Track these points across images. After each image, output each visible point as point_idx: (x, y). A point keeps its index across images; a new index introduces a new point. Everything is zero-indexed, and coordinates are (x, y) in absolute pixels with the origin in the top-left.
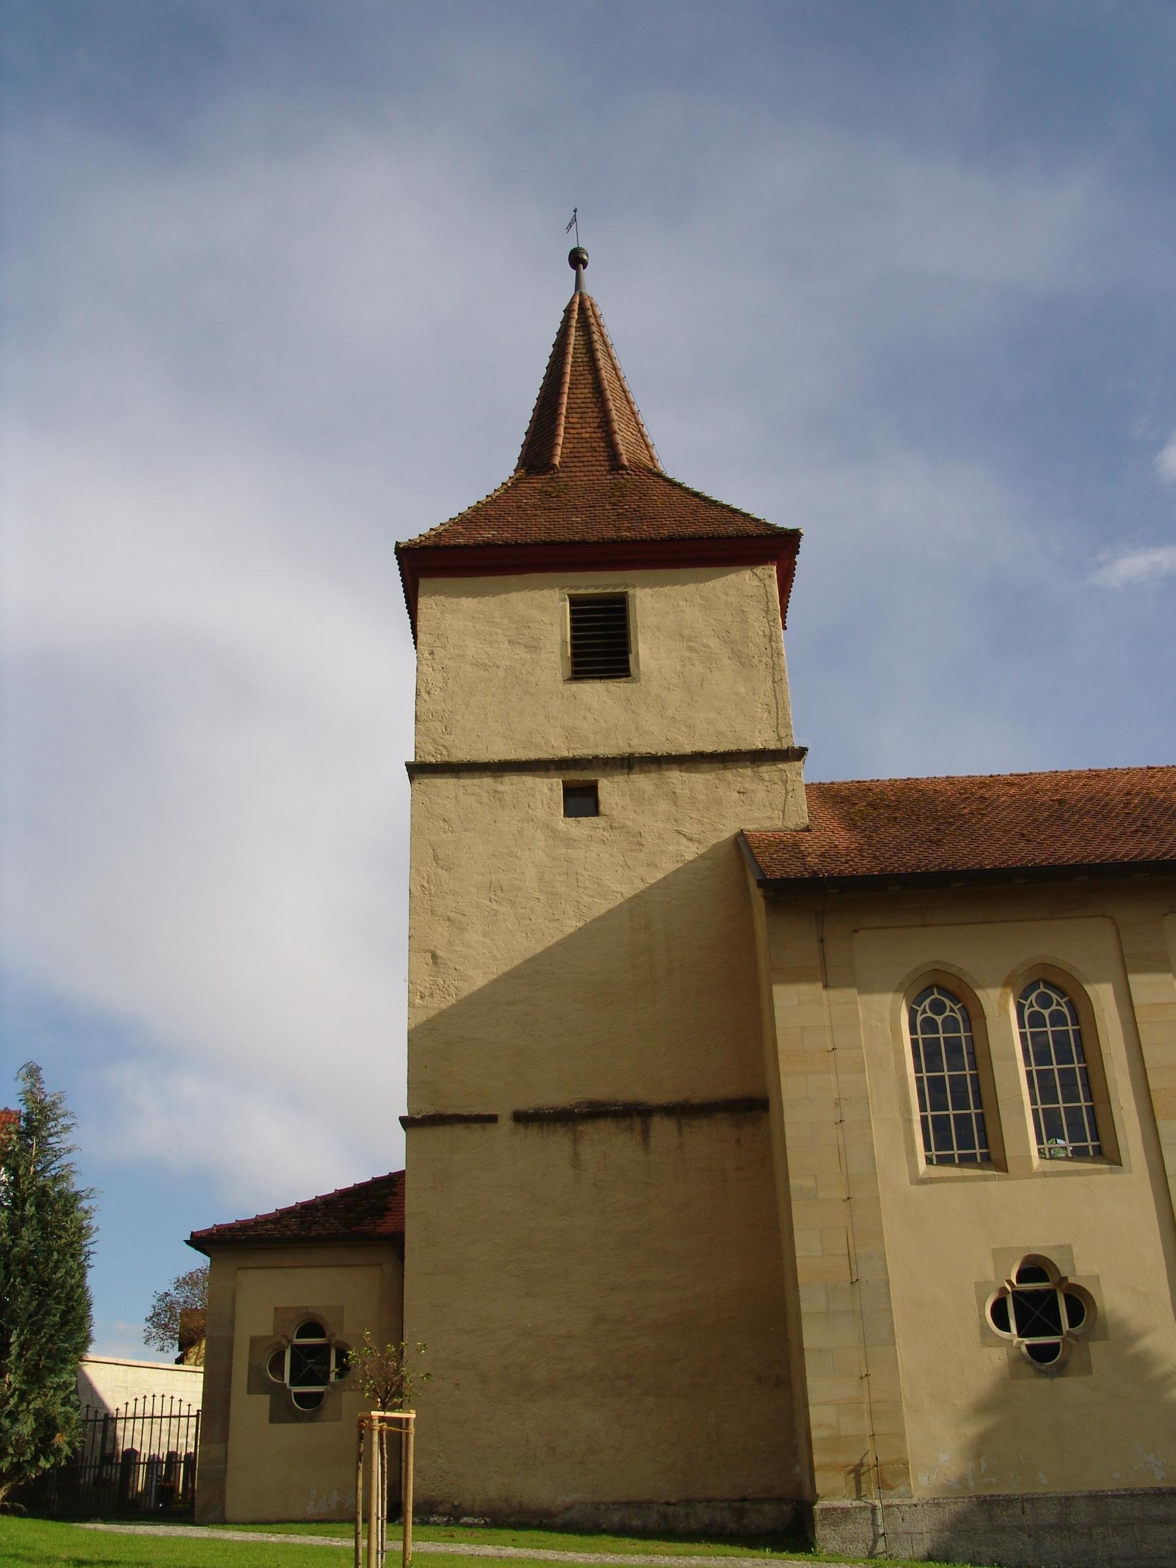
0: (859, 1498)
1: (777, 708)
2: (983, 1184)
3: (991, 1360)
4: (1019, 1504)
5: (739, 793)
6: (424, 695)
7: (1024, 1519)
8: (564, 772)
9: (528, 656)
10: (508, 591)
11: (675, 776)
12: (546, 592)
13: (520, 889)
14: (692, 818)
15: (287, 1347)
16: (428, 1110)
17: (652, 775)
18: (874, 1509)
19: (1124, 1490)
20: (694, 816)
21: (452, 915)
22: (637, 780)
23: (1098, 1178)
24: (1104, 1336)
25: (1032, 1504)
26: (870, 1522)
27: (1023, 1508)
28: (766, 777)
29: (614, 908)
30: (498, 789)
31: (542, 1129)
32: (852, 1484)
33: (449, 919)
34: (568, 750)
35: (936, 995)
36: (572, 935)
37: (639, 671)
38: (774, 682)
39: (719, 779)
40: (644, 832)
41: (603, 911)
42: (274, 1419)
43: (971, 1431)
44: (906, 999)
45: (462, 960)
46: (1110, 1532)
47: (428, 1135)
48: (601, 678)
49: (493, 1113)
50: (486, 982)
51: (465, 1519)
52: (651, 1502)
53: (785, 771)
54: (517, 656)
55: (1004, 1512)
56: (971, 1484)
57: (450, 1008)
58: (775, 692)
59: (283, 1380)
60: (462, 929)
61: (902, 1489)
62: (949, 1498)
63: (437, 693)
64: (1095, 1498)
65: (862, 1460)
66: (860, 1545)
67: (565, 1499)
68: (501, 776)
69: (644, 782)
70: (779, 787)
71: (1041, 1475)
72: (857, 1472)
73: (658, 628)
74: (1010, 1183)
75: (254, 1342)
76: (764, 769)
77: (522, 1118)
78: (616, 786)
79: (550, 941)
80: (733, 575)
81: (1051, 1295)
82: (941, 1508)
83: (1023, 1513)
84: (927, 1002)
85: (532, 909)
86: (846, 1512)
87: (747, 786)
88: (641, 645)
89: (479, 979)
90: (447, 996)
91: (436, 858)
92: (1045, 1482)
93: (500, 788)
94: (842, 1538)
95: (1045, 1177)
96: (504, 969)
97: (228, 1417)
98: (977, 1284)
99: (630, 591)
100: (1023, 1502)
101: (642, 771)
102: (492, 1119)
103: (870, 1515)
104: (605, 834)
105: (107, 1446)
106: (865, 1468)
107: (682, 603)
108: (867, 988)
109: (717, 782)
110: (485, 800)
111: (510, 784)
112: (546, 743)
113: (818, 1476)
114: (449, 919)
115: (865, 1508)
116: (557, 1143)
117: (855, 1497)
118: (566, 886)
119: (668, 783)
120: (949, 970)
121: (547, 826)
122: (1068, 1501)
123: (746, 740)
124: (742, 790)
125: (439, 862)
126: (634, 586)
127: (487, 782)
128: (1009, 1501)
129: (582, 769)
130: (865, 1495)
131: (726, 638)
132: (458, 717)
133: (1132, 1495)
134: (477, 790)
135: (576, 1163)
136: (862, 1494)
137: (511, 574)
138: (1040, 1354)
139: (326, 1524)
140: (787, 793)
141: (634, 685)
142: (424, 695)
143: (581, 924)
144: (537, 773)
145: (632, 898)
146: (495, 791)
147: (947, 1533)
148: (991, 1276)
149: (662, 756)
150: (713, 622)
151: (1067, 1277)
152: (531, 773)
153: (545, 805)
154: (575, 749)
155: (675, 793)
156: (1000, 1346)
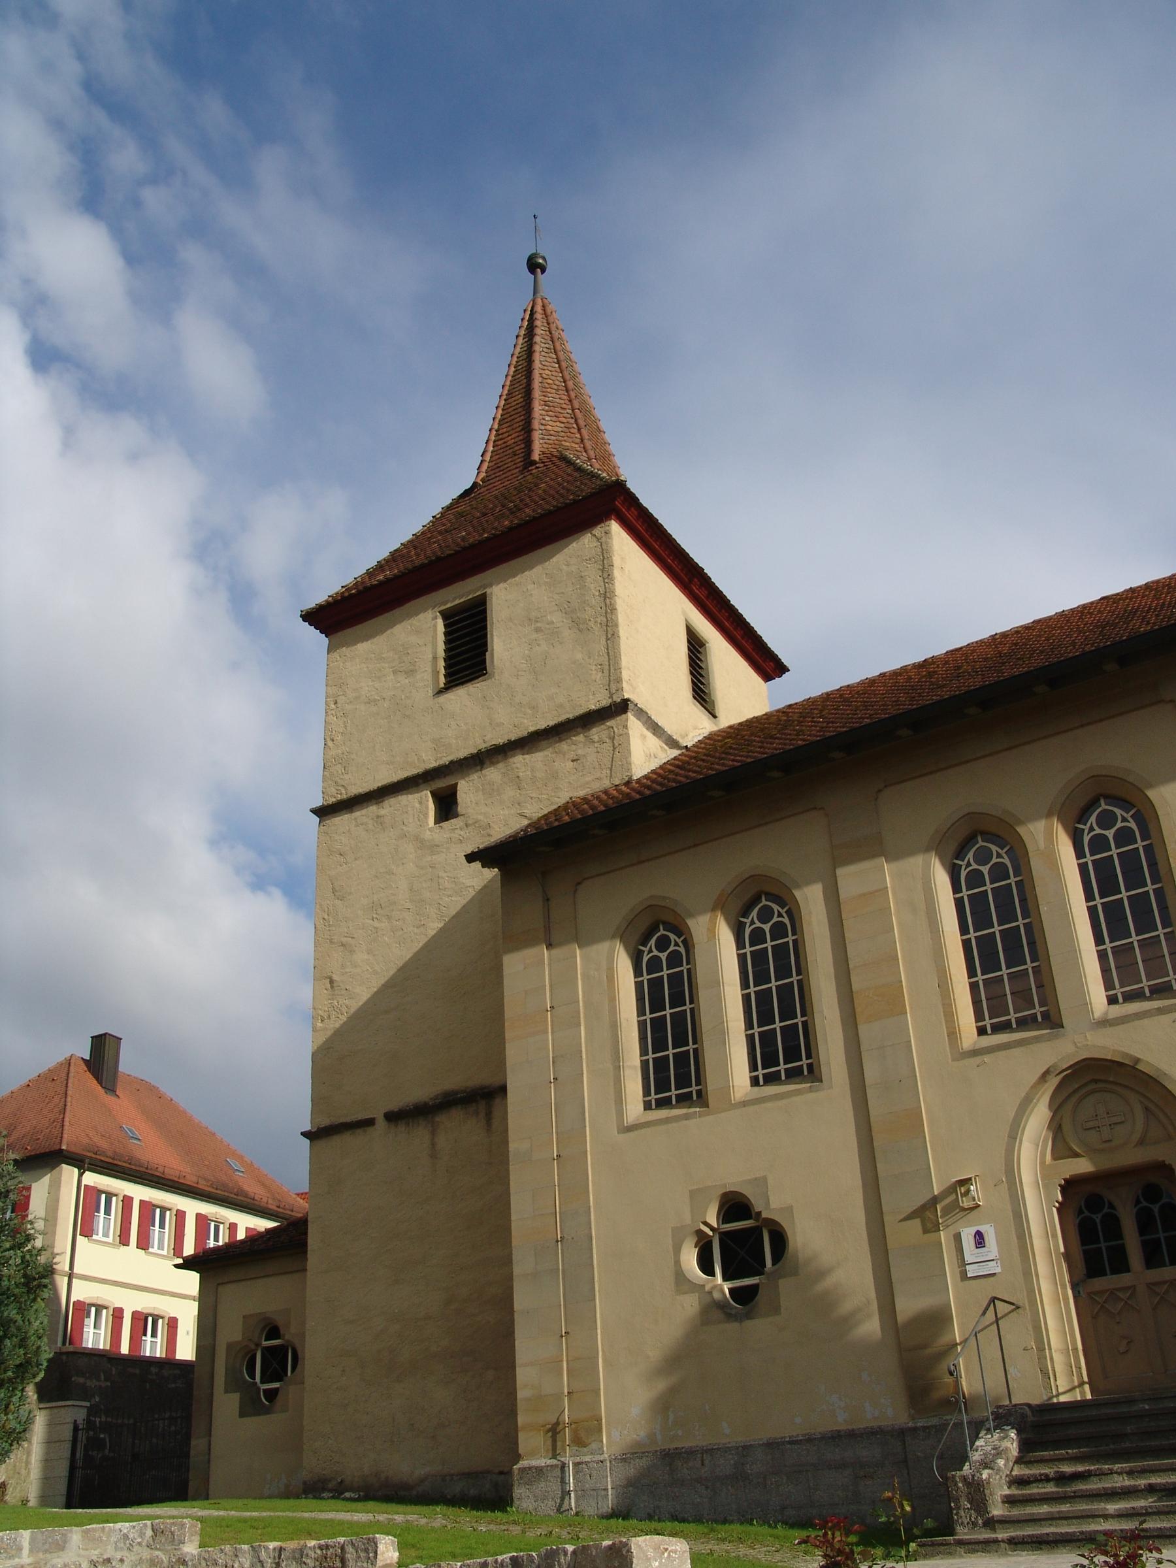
0: (554, 1456)
1: (609, 665)
2: (685, 1122)
3: (683, 1307)
4: (699, 1456)
5: (573, 761)
6: (330, 743)
7: (703, 1471)
8: (431, 783)
9: (407, 681)
10: (392, 625)
11: (519, 761)
12: (421, 616)
13: (395, 903)
14: (532, 798)
15: (257, 1350)
16: (325, 1122)
17: (500, 765)
18: (563, 1467)
19: (802, 1435)
20: (534, 795)
21: (344, 940)
22: (487, 773)
23: (797, 1099)
24: (794, 1272)
25: (711, 1455)
26: (559, 1480)
27: (702, 1461)
28: (596, 738)
29: (467, 903)
30: (379, 814)
31: (409, 1126)
32: (549, 1442)
33: (343, 945)
34: (436, 761)
35: (662, 932)
36: (434, 936)
37: (494, 666)
38: (607, 639)
39: (556, 752)
40: (493, 822)
41: (459, 907)
42: (242, 1414)
43: (661, 1385)
44: (624, 944)
45: (351, 980)
46: (784, 1481)
47: (322, 1144)
48: (462, 683)
49: (372, 1116)
50: (369, 996)
51: (347, 1495)
52: (488, 1472)
53: (612, 727)
54: (399, 684)
55: (685, 1465)
56: (659, 1437)
57: (342, 1026)
58: (608, 649)
59: (255, 1379)
60: (352, 952)
61: (594, 1446)
62: (636, 1453)
63: (339, 738)
64: (772, 1445)
65: (558, 1419)
66: (550, 1503)
67: (420, 1472)
68: (382, 802)
69: (493, 773)
70: (608, 746)
71: (725, 1425)
72: (554, 1431)
73: (511, 619)
74: (710, 1118)
75: (229, 1346)
76: (594, 730)
77: (393, 1117)
78: (471, 784)
79: (417, 947)
80: (574, 544)
81: (755, 1232)
82: (627, 1464)
83: (703, 1465)
84: (653, 942)
85: (404, 920)
86: (539, 1471)
87: (580, 752)
88: (496, 640)
89: (363, 994)
90: (340, 1016)
91: (334, 891)
92: (729, 1433)
93: (382, 812)
94: (535, 1496)
95: (744, 1106)
96: (383, 981)
97: (211, 1415)
98: (673, 1229)
99: (488, 591)
100: (702, 1454)
101: (493, 764)
102: (369, 1123)
103: (559, 1473)
104: (462, 833)
105: (193, 1443)
106: (561, 1427)
107: (530, 587)
108: (583, 940)
109: (554, 755)
110: (371, 826)
111: (391, 807)
112: (418, 759)
113: (522, 1436)
114: (343, 945)
115: (556, 1466)
116: (417, 1136)
117: (550, 1456)
118: (430, 892)
119: (512, 769)
120: (663, 904)
121: (417, 838)
122: (745, 1450)
123: (581, 706)
124: (575, 758)
125: (336, 894)
126: (491, 585)
127: (372, 810)
128: (691, 1452)
129: (445, 777)
130: (559, 1454)
131: (567, 609)
132: (354, 756)
133: (810, 1439)
134: (365, 819)
135: (434, 1155)
136: (558, 1452)
137: (395, 609)
138: (743, 1296)
139: (394, 1505)
140: (614, 749)
141: (489, 681)
142: (330, 743)
143: (441, 925)
144: (411, 790)
145: (481, 889)
146: (378, 817)
147: (631, 1489)
148: (688, 1221)
149: (504, 745)
150: (556, 596)
151: (761, 1212)
152: (405, 792)
153: (416, 820)
154: (441, 758)
155: (518, 777)
156: (693, 1293)
